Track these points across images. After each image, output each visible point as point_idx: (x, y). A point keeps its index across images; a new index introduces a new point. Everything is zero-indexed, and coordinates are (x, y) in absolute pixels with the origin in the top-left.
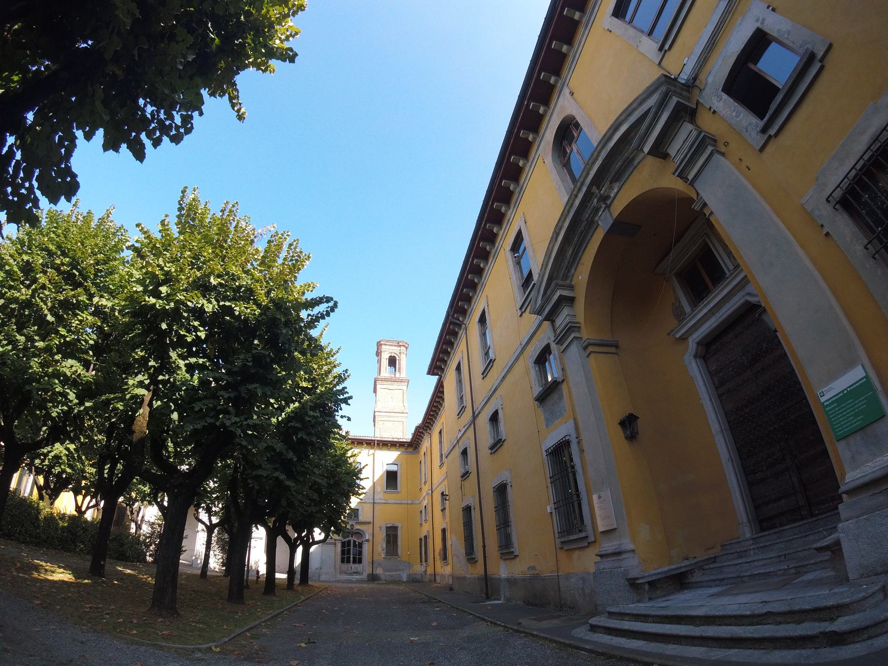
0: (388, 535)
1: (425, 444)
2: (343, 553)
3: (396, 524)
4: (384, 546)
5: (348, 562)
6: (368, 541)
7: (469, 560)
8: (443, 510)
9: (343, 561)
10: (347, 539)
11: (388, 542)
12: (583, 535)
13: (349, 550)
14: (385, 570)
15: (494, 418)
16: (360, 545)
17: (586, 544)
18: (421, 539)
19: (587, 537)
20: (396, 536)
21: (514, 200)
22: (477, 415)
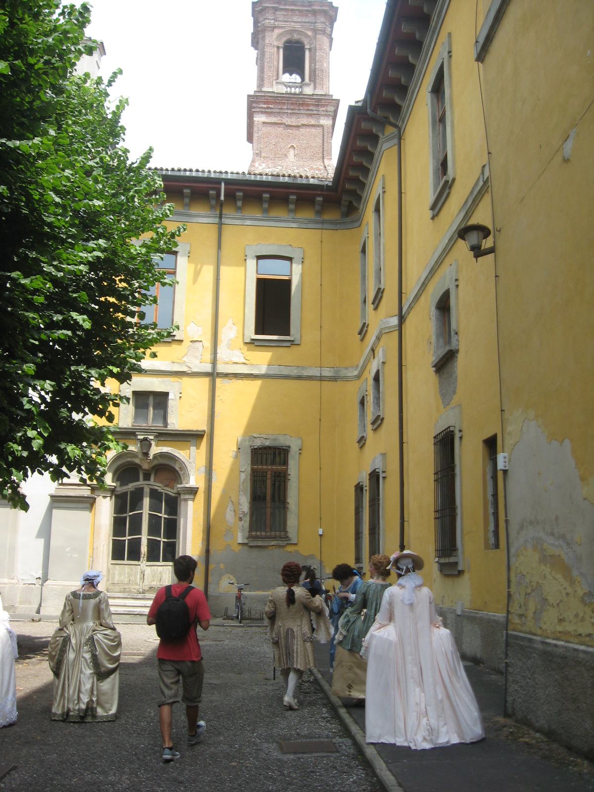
0: (257, 479)
1: (382, 179)
2: (119, 525)
3: (282, 441)
4: (245, 506)
5: (135, 555)
6: (193, 491)
7: (442, 567)
8: (444, 364)
9: (118, 553)
10: (131, 486)
11: (257, 498)
12: (452, 560)
13: (154, 529)
14: (356, 583)
15: (444, 306)
16: (173, 506)
17: (456, 573)
18: (359, 488)
19: (457, 563)
20: (281, 480)
21: (433, 24)
22: (408, 312)
